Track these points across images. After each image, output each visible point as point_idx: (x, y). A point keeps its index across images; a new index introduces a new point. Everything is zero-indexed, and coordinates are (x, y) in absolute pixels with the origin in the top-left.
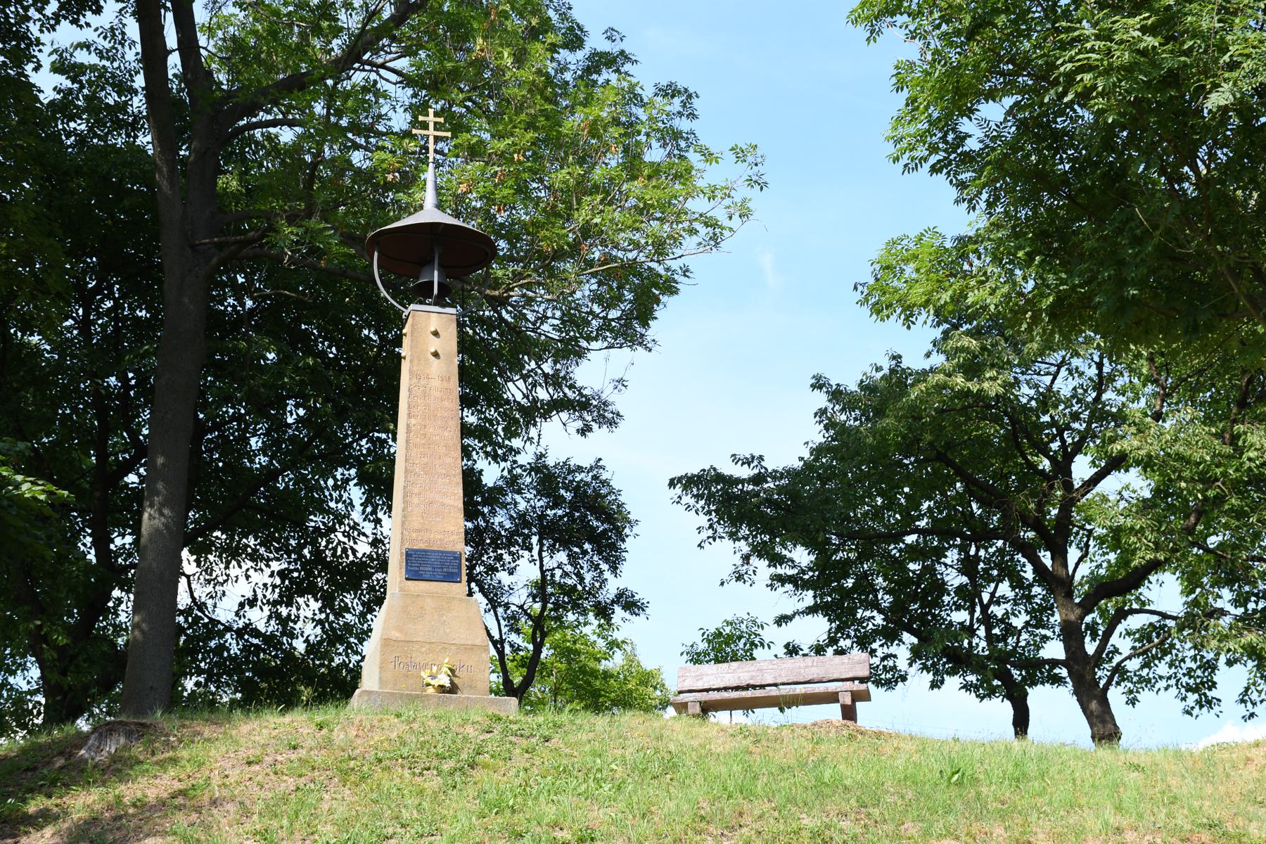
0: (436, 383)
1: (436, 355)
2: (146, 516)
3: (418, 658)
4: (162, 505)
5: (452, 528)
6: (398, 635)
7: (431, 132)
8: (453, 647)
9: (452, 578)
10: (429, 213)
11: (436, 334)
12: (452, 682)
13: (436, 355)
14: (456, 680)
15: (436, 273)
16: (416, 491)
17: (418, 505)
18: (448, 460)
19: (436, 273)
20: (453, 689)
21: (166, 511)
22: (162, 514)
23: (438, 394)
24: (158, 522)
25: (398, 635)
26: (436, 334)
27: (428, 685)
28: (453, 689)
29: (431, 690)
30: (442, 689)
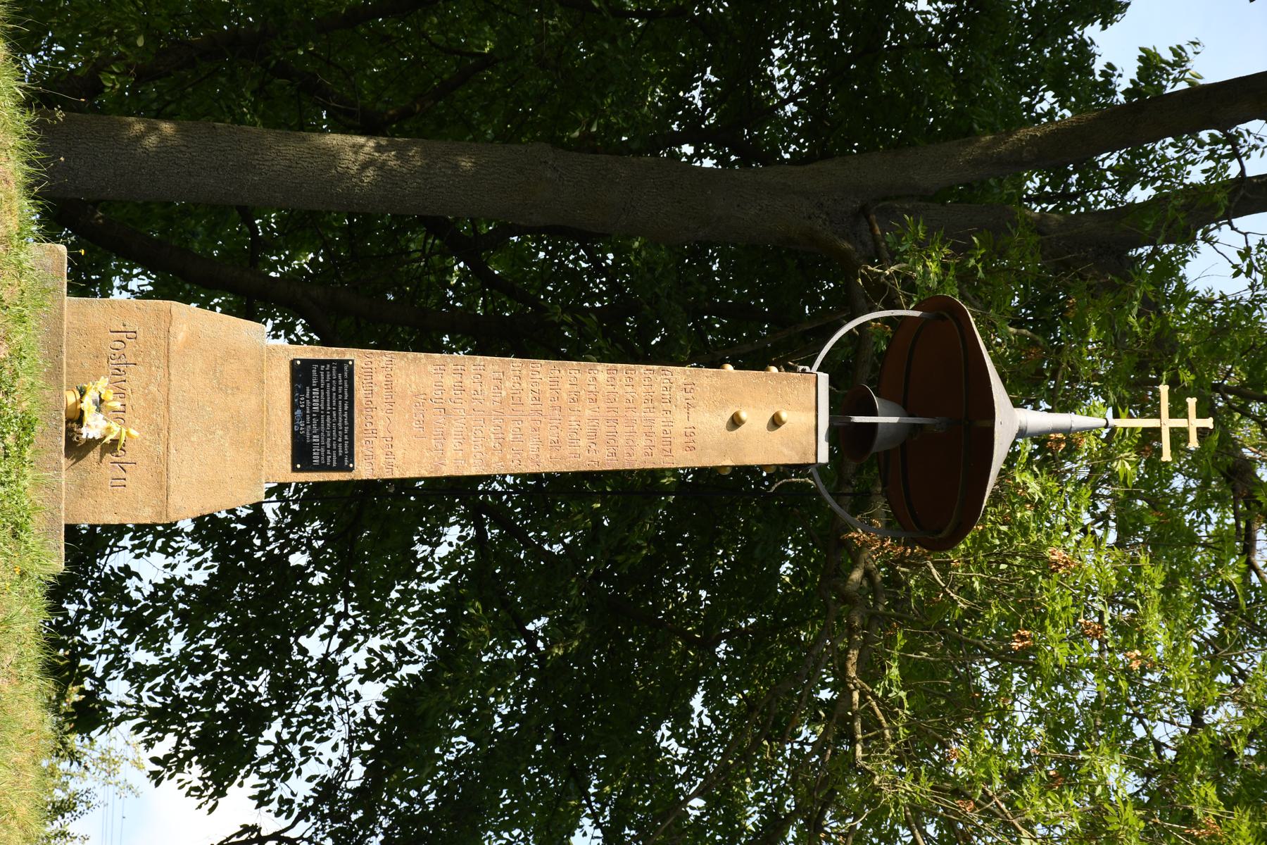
0: (680, 422)
1: (735, 422)
2: (361, 140)
3: (134, 378)
4: (382, 167)
5: (399, 453)
6: (181, 337)
7: (1166, 423)
8: (161, 448)
9: (302, 455)
10: (1012, 420)
11: (776, 422)
12: (91, 443)
13: (735, 422)
14: (94, 455)
15: (895, 420)
16: (467, 382)
17: (439, 385)
18: (531, 445)
19: (895, 420)
20: (76, 448)
21: (370, 172)
22: (365, 166)
23: (658, 428)
24: (350, 161)
25: (181, 337)
26: (776, 422)
27: (83, 393)
28: (76, 448)
29: (71, 398)
30: (77, 419)
